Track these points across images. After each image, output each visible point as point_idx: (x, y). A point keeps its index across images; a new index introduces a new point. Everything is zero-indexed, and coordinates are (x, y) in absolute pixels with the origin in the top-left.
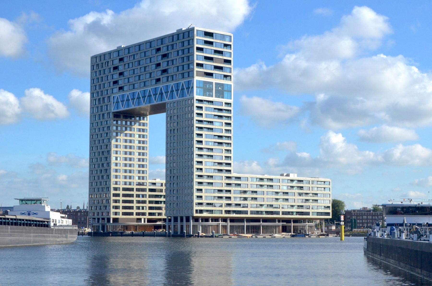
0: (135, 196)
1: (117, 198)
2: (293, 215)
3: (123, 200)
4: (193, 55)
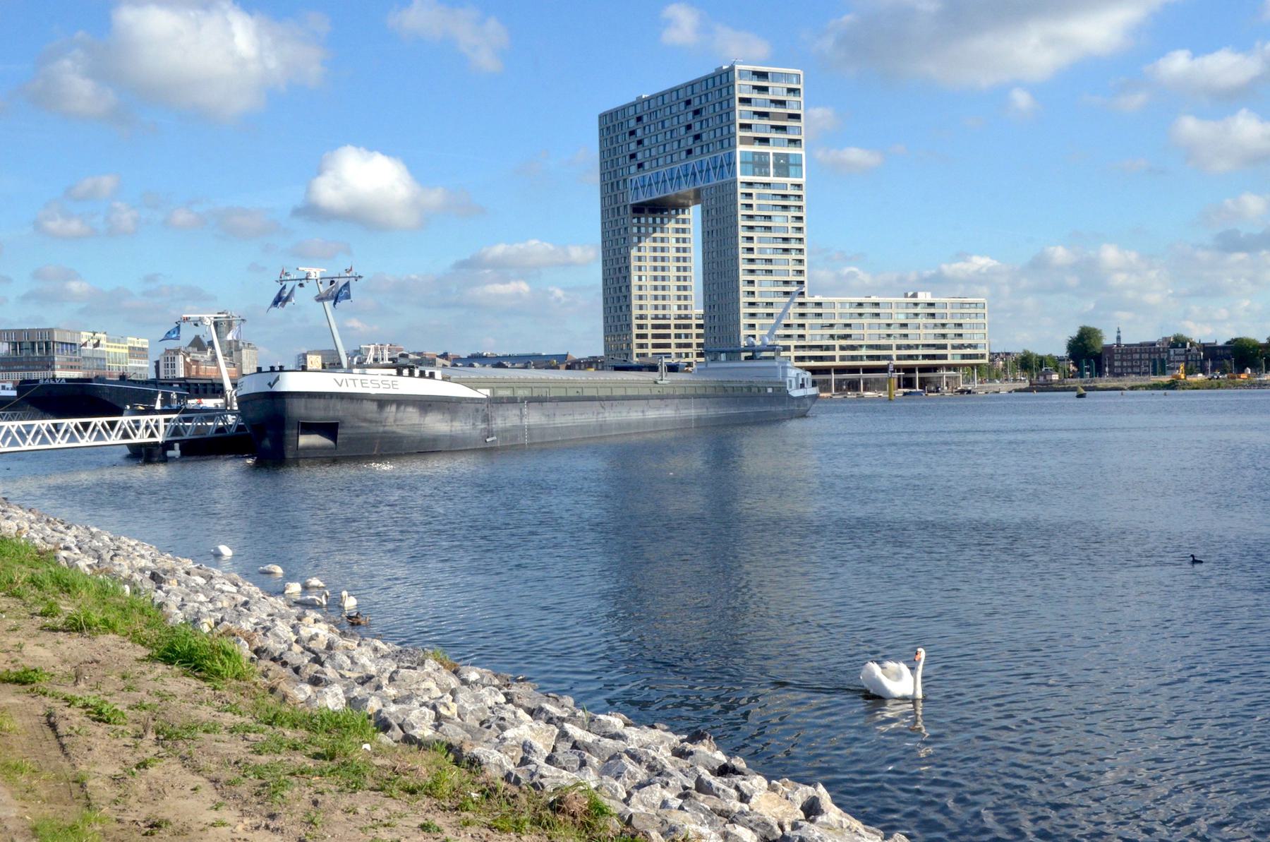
0: (673, 336)
1: (643, 341)
2: (917, 359)
3: (653, 344)
4: (734, 110)
